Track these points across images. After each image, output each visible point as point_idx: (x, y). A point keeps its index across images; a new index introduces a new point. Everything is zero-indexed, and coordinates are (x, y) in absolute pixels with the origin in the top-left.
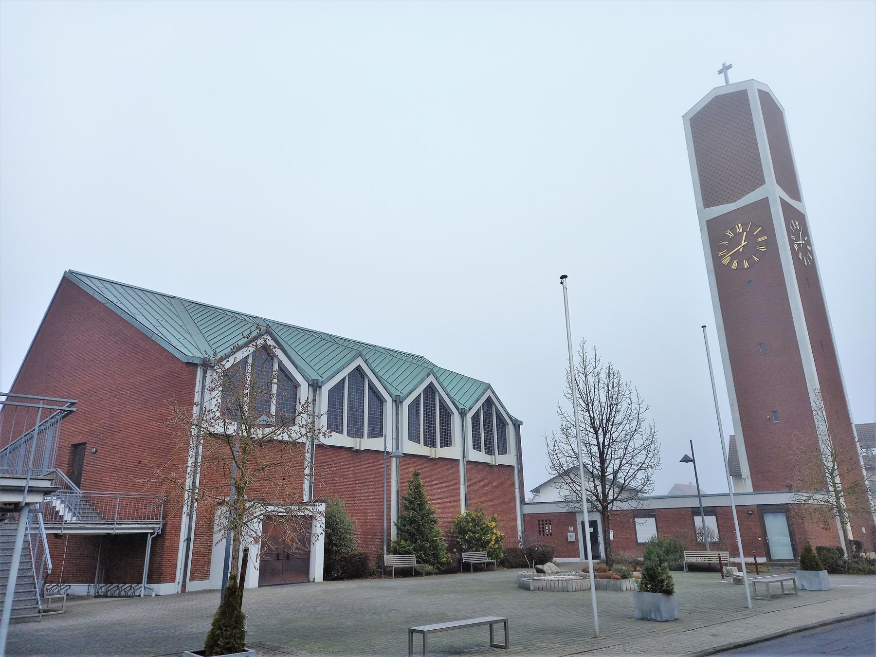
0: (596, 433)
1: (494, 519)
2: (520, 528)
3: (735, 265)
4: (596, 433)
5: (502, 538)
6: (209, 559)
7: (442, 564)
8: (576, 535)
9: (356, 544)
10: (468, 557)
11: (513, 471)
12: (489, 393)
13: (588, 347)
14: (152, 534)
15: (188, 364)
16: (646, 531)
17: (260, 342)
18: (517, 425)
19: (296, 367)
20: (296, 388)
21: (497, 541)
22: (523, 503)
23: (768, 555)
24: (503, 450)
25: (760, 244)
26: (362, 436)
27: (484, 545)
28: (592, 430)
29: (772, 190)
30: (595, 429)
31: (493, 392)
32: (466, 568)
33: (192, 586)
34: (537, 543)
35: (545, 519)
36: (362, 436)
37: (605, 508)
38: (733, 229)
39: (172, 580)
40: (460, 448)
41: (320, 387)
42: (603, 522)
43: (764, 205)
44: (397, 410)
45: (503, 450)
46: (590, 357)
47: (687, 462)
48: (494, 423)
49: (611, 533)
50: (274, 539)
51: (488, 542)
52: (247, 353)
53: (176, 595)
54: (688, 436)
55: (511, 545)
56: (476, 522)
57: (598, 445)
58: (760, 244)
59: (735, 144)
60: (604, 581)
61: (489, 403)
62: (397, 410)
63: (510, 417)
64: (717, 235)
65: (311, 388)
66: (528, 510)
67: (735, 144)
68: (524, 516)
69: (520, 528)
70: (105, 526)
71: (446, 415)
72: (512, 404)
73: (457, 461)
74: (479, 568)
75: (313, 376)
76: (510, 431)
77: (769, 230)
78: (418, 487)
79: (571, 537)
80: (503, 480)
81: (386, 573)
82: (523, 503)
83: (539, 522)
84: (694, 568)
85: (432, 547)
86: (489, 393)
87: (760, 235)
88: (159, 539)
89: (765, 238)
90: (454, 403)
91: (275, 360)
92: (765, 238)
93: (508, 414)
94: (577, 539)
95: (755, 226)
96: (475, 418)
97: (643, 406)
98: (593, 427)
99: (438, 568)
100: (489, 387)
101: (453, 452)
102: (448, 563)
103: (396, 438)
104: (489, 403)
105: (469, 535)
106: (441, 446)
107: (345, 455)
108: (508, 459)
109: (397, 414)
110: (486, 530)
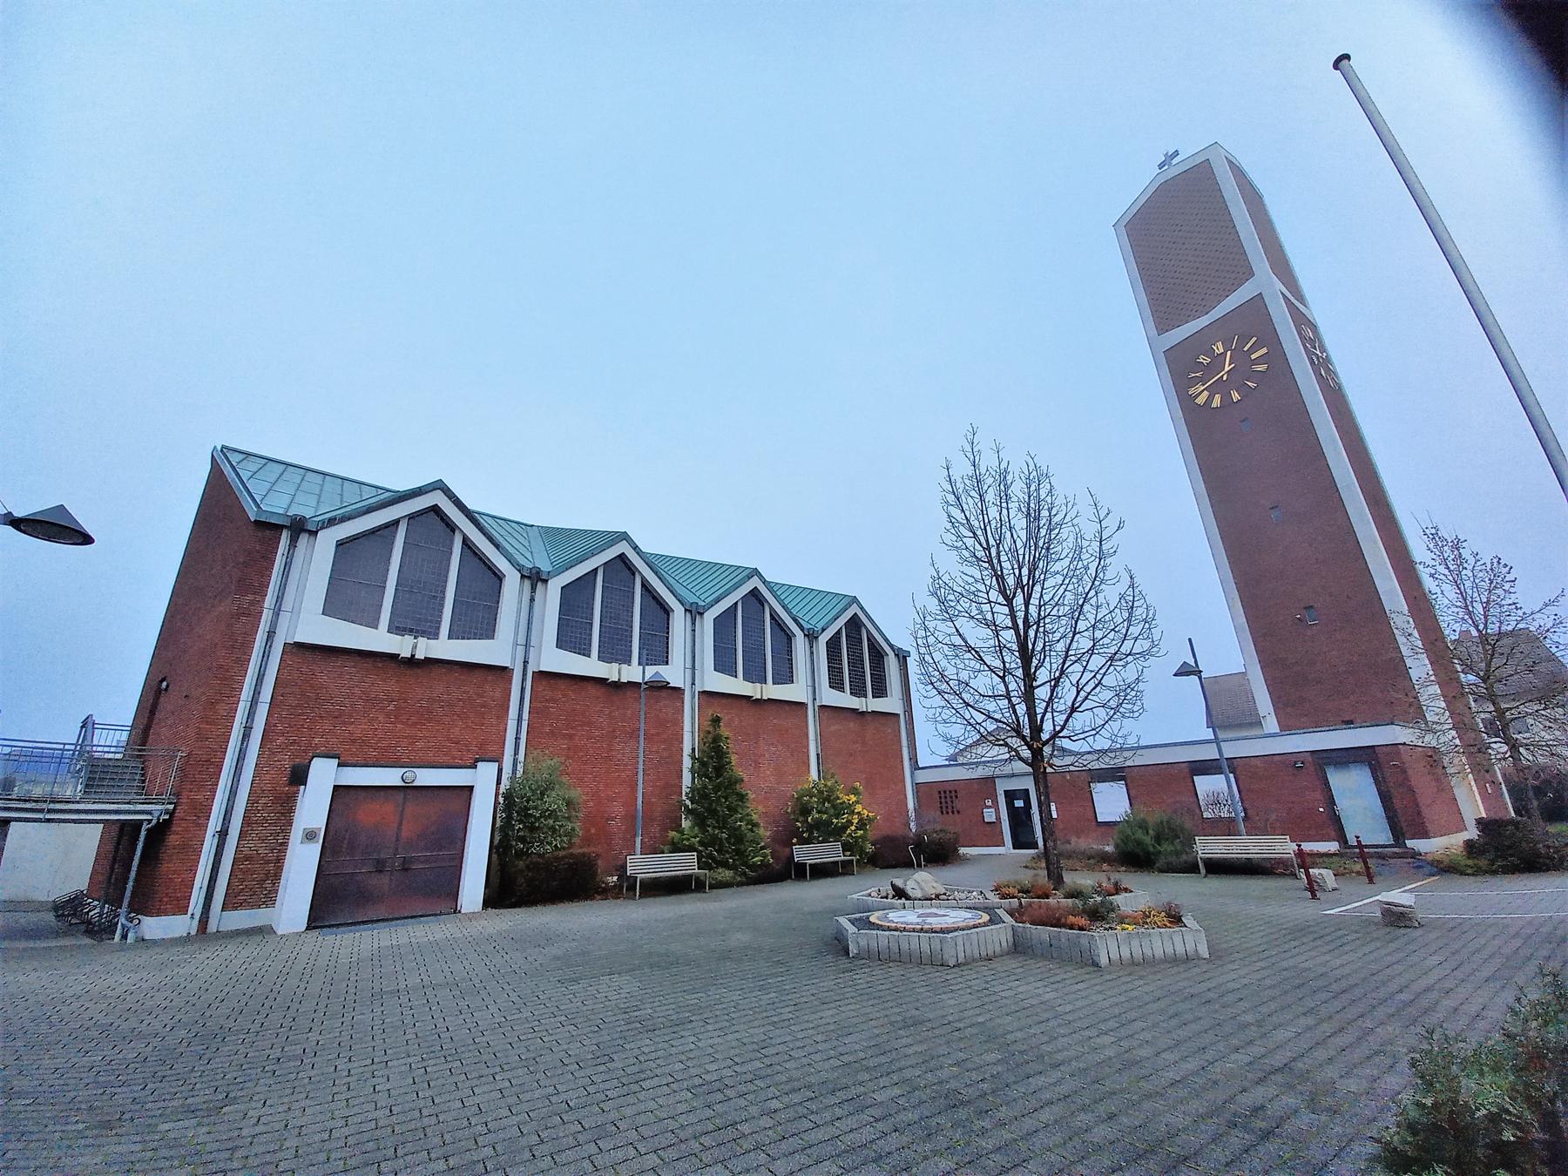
0: (1009, 602)
1: (855, 791)
2: (911, 805)
3: (1217, 402)
4: (1009, 602)
5: (870, 820)
6: (281, 868)
7: (753, 867)
9: (569, 838)
10: (805, 854)
12: (854, 609)
13: (984, 444)
14: (150, 821)
15: (260, 525)
16: (1111, 803)
18: (902, 657)
19: (497, 546)
21: (862, 825)
22: (915, 766)
23: (1342, 838)
24: (880, 691)
25: (1256, 362)
27: (834, 833)
28: (1001, 599)
29: (1264, 281)
30: (1006, 597)
31: (862, 608)
32: (799, 872)
33: (223, 920)
34: (939, 825)
36: (629, 662)
37: (1037, 754)
38: (1209, 352)
39: (183, 910)
40: (808, 683)
41: (545, 581)
42: (1038, 790)
43: (1258, 301)
44: (694, 623)
45: (880, 691)
46: (988, 461)
47: (1188, 674)
48: (859, 652)
49: (1053, 807)
51: (845, 828)
53: (187, 940)
54: (1174, 647)
55: (887, 831)
56: (827, 797)
57: (1015, 627)
58: (1256, 362)
59: (1194, 246)
60: (1044, 933)
61: (854, 624)
62: (694, 623)
63: (891, 646)
64: (1183, 368)
65: (527, 583)
66: (922, 777)
67: (1194, 246)
68: (918, 787)
69: (911, 805)
70: (126, 807)
71: (784, 636)
72: (894, 624)
73: (802, 705)
74: (822, 871)
76: (892, 664)
77: (1271, 338)
78: (717, 739)
79: (989, 815)
80: (882, 737)
81: (628, 888)
83: (944, 796)
84: (1218, 868)
85: (728, 841)
86: (854, 609)
87: (1253, 349)
88: (160, 831)
89: (1264, 350)
90: (795, 620)
92: (1264, 350)
93: (886, 640)
94: (998, 818)
95: (1244, 339)
96: (833, 645)
97: (1111, 523)
98: (1003, 592)
99: (744, 874)
100: (855, 600)
101: (793, 692)
102: (764, 865)
103: (690, 664)
104: (854, 624)
105: (814, 818)
107: (593, 690)
108: (891, 704)
110: (839, 809)
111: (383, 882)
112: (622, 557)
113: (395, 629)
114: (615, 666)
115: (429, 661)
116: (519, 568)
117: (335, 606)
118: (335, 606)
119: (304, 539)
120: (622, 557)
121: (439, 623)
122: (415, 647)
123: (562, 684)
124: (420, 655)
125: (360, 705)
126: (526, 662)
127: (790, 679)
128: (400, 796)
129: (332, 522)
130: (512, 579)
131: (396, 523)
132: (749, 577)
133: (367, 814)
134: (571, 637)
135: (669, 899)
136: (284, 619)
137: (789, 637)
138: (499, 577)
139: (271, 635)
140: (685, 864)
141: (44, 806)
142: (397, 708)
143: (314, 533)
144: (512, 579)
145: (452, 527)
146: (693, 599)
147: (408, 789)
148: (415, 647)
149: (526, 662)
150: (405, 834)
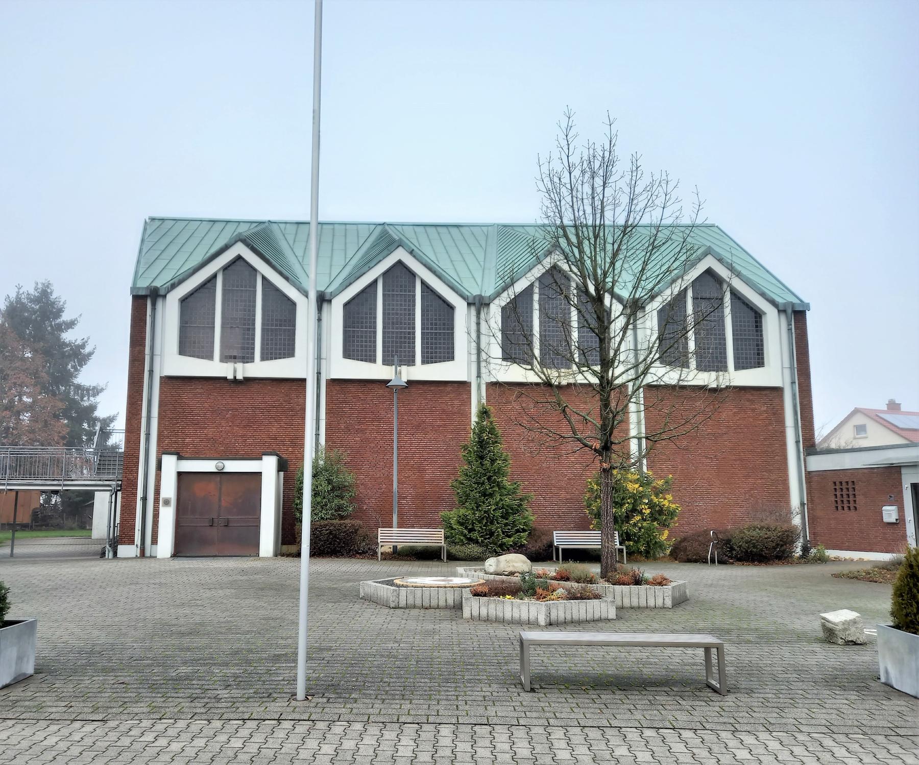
8: (901, 510)
11: (469, 393)
17: (548, 263)
18: (797, 316)
20: (760, 317)
22: (810, 447)
26: (685, 365)
35: (844, 480)
41: (330, 301)
44: (478, 317)
45: (287, 350)
50: (697, 602)
52: (533, 279)
65: (783, 318)
66: (817, 463)
68: (812, 479)
75: (474, 291)
82: (810, 447)
91: (725, 286)
103: (318, 355)
106: (423, 362)
108: (773, 372)
109: (319, 320)
111: (214, 533)
112: (709, 272)
113: (225, 358)
114: (714, 374)
115: (247, 380)
116: (773, 303)
117: (185, 349)
118: (185, 349)
119: (160, 303)
120: (709, 272)
121: (253, 349)
122: (235, 371)
123: (352, 388)
124: (240, 377)
125: (209, 415)
126: (319, 373)
127: (449, 355)
128: (218, 478)
129: (173, 286)
130: (460, 306)
131: (214, 276)
132: (705, 254)
133: (199, 489)
134: (356, 345)
135: (417, 563)
136: (157, 360)
137: (758, 315)
138: (451, 308)
139: (151, 372)
140: (435, 537)
141: (61, 482)
142: (234, 416)
143: (165, 296)
144: (460, 306)
145: (413, 275)
146: (476, 292)
147: (220, 474)
148: (235, 371)
149: (319, 373)
150: (223, 504)
